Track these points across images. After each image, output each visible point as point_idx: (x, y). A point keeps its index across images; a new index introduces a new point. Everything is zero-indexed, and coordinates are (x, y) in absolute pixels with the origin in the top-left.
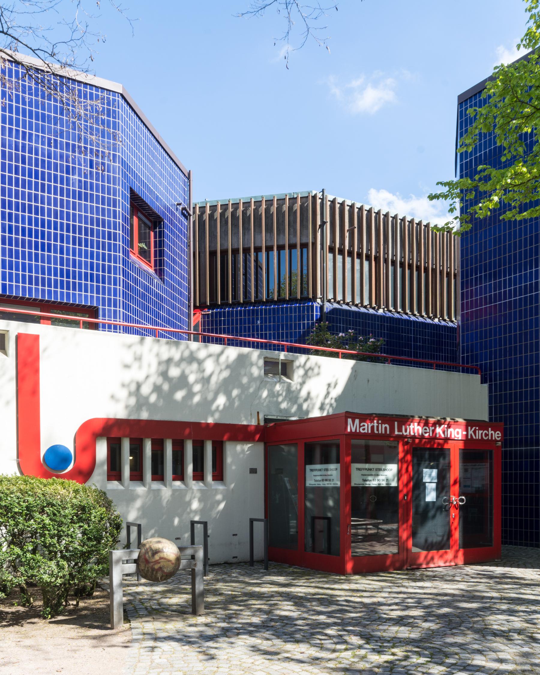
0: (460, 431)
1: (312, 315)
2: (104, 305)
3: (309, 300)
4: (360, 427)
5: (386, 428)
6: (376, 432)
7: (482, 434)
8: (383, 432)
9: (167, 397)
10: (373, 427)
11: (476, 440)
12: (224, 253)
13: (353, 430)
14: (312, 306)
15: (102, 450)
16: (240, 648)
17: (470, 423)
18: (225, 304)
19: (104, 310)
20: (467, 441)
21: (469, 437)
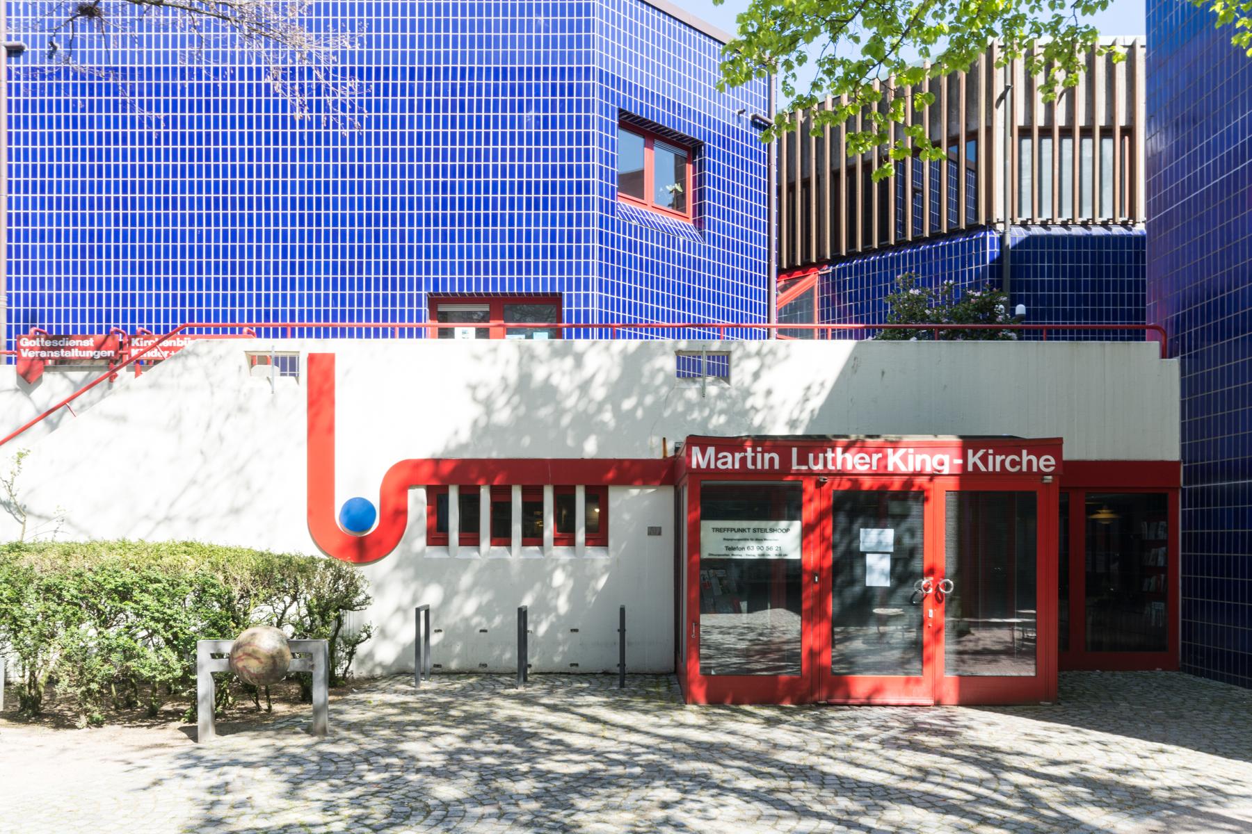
0: (946, 458)
1: (984, 255)
2: (570, 289)
3: (983, 228)
4: (717, 459)
5: (772, 460)
6: (750, 466)
7: (1003, 462)
8: (737, 466)
9: (522, 424)
10: (743, 460)
11: (987, 474)
12: (851, 171)
13: (703, 466)
14: (984, 239)
15: (417, 500)
16: (437, 795)
17: (969, 443)
18: (852, 255)
19: (570, 296)
20: (964, 475)
21: (970, 469)
